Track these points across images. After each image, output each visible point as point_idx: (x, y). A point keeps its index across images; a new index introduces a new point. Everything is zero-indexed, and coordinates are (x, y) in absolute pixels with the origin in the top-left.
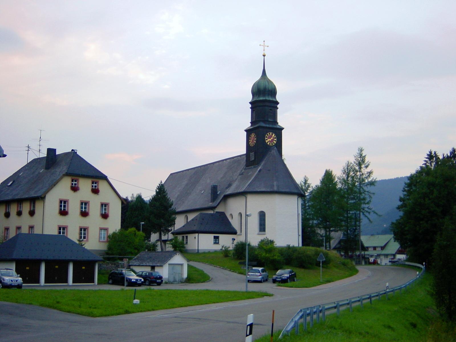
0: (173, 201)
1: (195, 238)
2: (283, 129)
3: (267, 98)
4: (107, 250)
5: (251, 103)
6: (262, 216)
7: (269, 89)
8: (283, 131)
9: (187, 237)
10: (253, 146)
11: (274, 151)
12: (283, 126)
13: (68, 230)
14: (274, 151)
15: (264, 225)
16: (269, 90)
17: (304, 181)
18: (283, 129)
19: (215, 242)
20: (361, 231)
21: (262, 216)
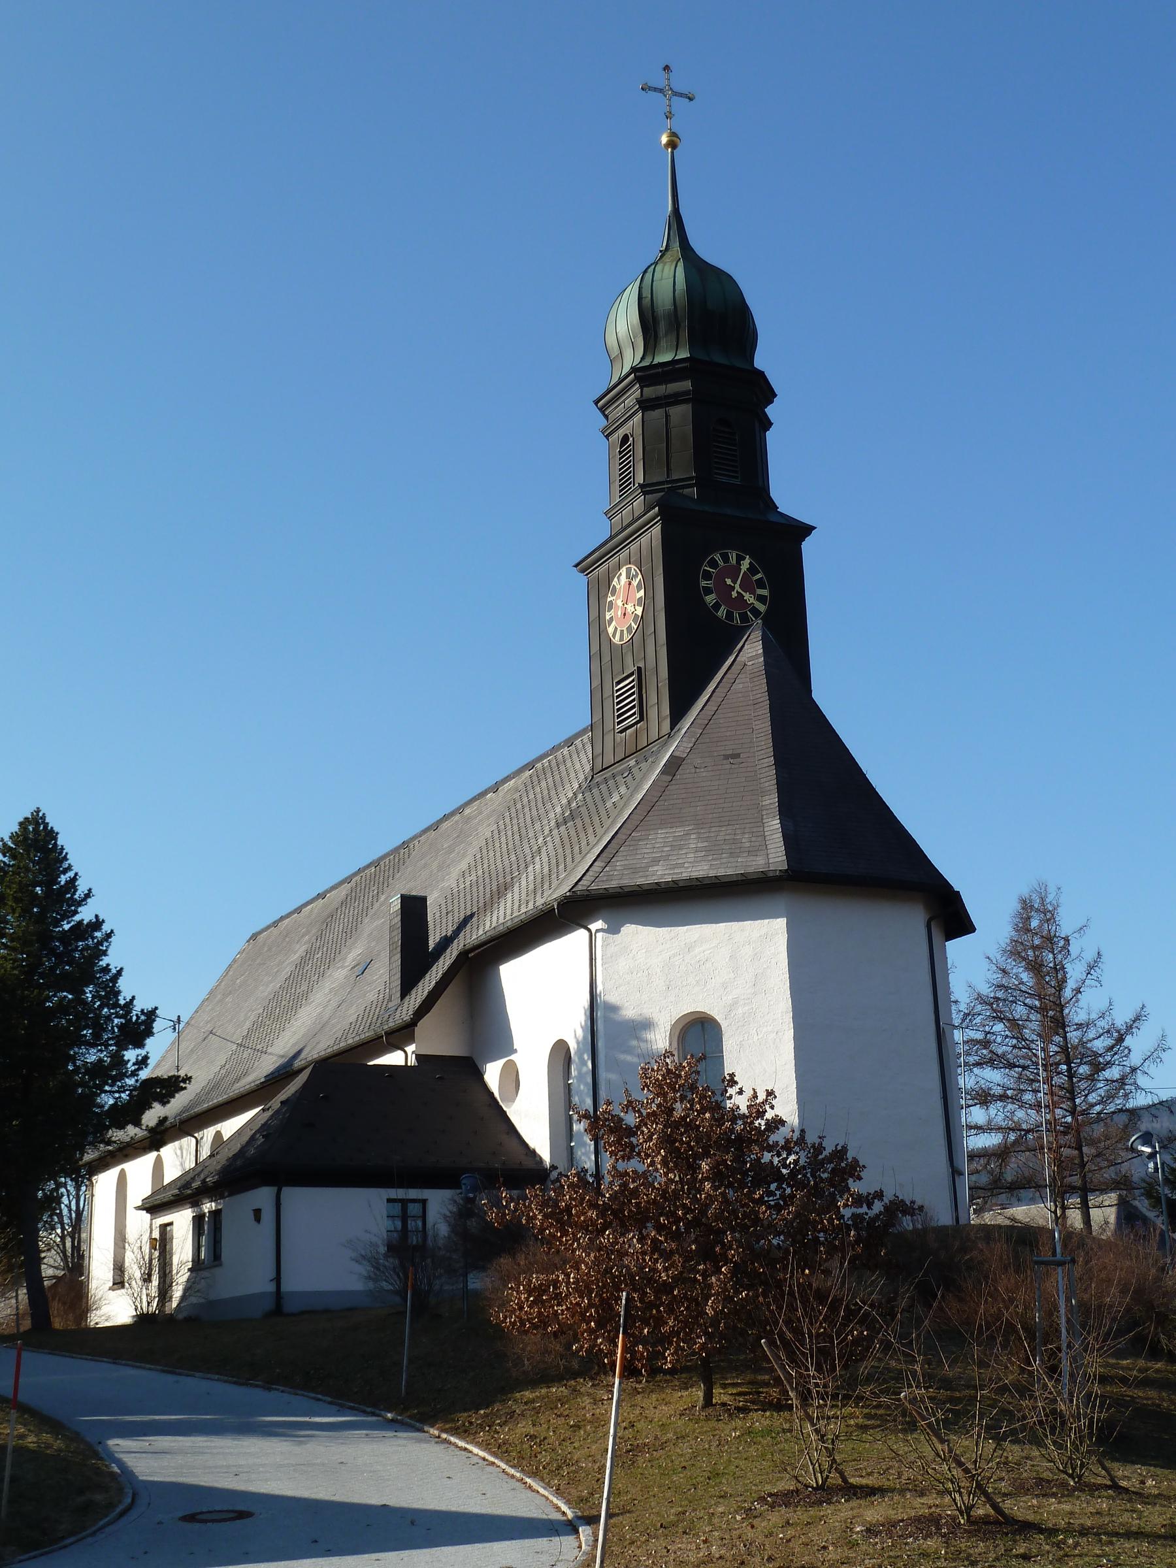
1: (257, 1214)
10: (627, 637)
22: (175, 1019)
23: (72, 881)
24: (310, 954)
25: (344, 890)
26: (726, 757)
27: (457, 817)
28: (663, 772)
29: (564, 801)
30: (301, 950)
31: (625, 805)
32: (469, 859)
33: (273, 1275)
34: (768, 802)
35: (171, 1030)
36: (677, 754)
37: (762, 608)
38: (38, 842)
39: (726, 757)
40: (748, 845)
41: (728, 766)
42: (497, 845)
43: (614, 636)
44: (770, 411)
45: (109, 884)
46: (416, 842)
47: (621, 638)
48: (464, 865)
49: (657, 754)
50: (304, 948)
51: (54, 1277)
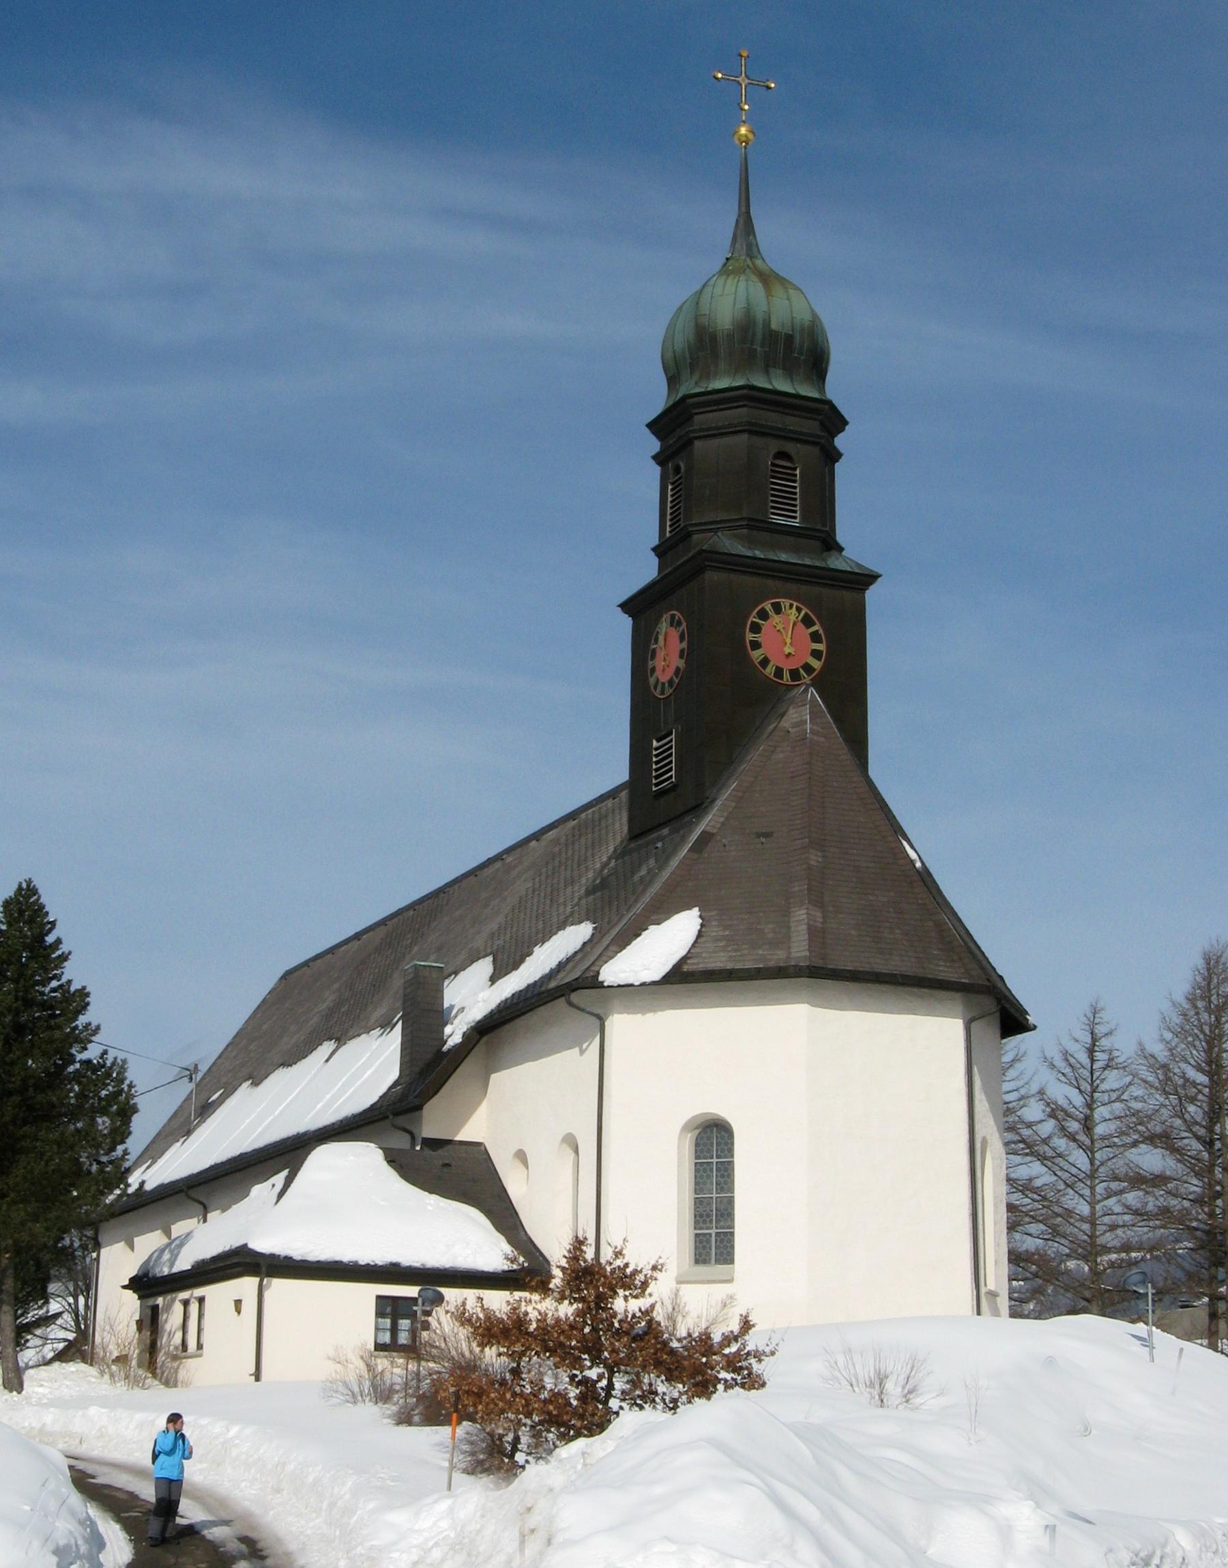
0: (115, 1059)
1: (238, 1303)
2: (871, 578)
3: (760, 382)
4: (501, 1321)
5: (656, 426)
6: (713, 1141)
7: (774, 326)
8: (872, 595)
9: (201, 1300)
10: (669, 691)
11: (803, 714)
12: (870, 563)
13: (447, 1266)
14: (803, 714)
15: (726, 1212)
16: (771, 337)
17: (1088, 1039)
18: (871, 578)
19: (386, 1338)
20: (671, 1318)
21: (713, 1141)
22: (192, 1068)
23: (59, 941)
24: (338, 1004)
25: (382, 932)
26: (759, 835)
27: (498, 865)
28: (690, 850)
29: (598, 866)
30: (329, 998)
31: (651, 882)
32: (500, 919)
33: (253, 1370)
34: (796, 889)
35: (186, 1079)
36: (708, 829)
37: (816, 664)
38: (26, 907)
39: (759, 835)
40: (770, 936)
41: (759, 846)
42: (529, 905)
43: (655, 688)
44: (840, 441)
45: (88, 960)
46: (456, 887)
47: (662, 693)
48: (494, 926)
49: (691, 826)
50: (332, 997)
51: (65, 1340)
